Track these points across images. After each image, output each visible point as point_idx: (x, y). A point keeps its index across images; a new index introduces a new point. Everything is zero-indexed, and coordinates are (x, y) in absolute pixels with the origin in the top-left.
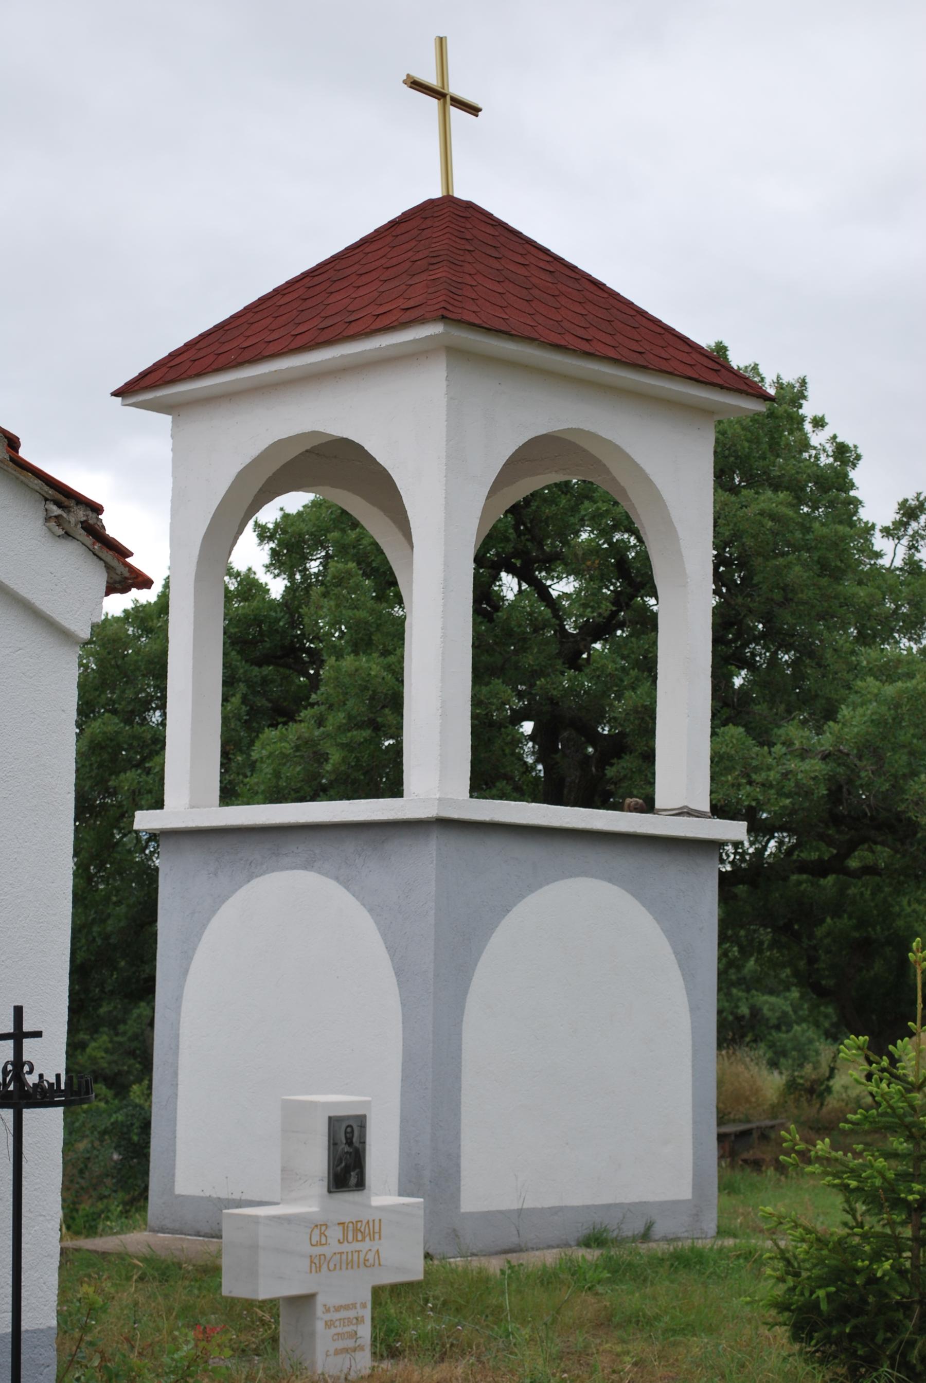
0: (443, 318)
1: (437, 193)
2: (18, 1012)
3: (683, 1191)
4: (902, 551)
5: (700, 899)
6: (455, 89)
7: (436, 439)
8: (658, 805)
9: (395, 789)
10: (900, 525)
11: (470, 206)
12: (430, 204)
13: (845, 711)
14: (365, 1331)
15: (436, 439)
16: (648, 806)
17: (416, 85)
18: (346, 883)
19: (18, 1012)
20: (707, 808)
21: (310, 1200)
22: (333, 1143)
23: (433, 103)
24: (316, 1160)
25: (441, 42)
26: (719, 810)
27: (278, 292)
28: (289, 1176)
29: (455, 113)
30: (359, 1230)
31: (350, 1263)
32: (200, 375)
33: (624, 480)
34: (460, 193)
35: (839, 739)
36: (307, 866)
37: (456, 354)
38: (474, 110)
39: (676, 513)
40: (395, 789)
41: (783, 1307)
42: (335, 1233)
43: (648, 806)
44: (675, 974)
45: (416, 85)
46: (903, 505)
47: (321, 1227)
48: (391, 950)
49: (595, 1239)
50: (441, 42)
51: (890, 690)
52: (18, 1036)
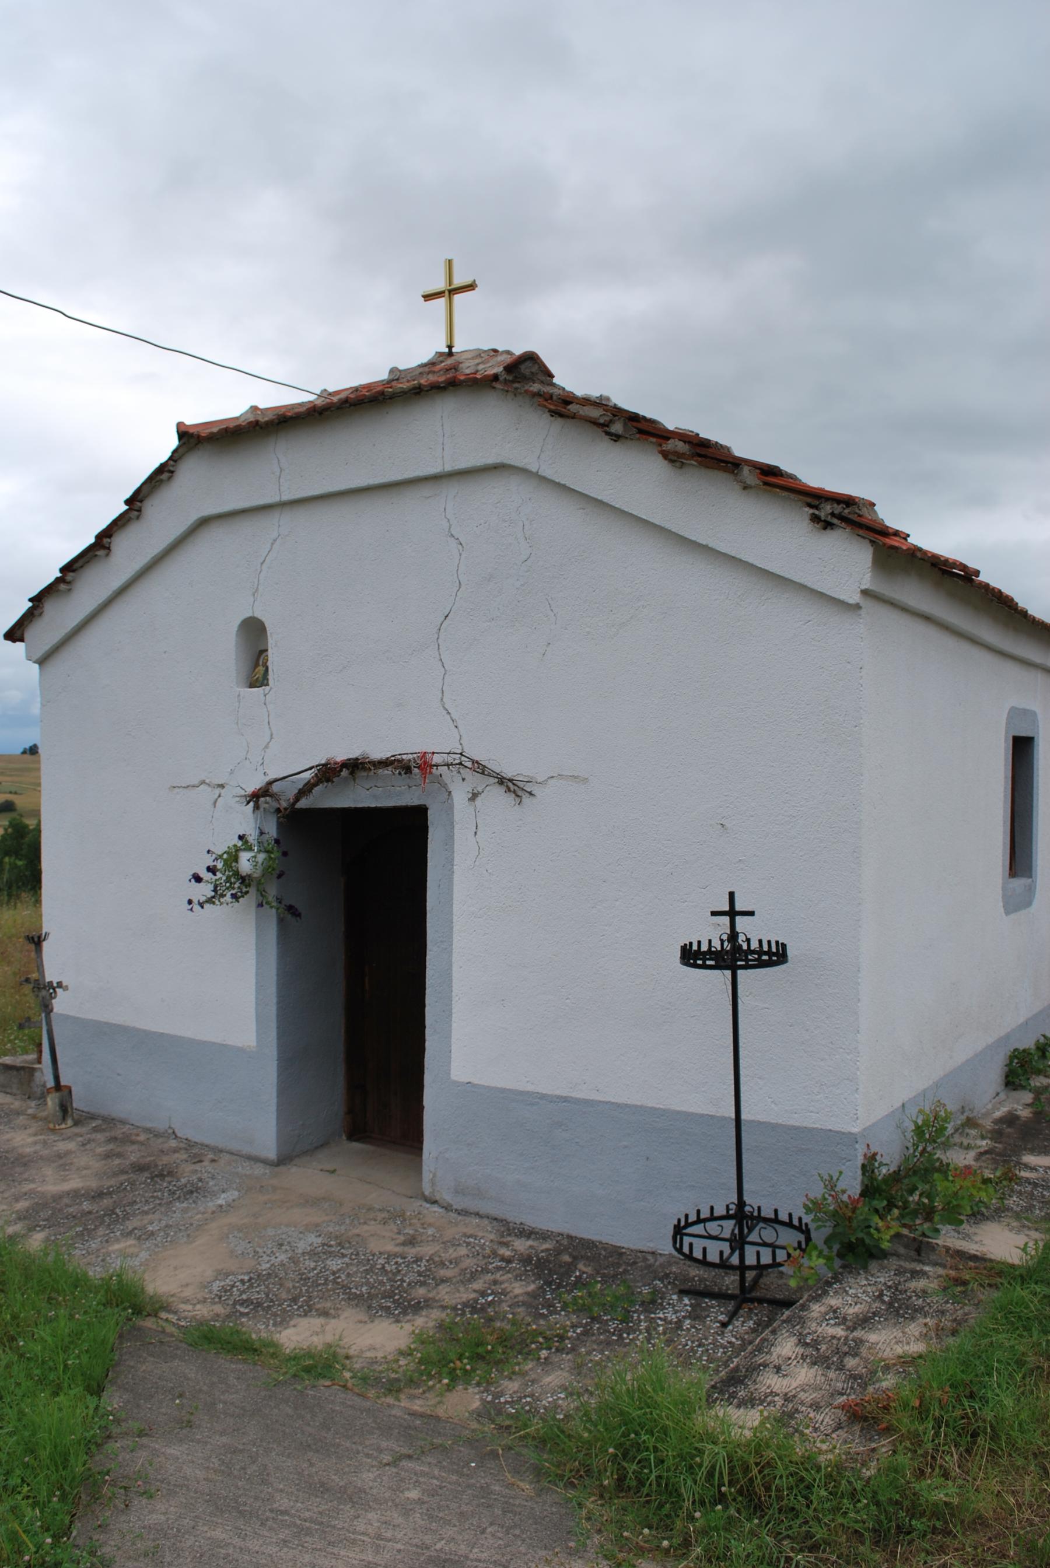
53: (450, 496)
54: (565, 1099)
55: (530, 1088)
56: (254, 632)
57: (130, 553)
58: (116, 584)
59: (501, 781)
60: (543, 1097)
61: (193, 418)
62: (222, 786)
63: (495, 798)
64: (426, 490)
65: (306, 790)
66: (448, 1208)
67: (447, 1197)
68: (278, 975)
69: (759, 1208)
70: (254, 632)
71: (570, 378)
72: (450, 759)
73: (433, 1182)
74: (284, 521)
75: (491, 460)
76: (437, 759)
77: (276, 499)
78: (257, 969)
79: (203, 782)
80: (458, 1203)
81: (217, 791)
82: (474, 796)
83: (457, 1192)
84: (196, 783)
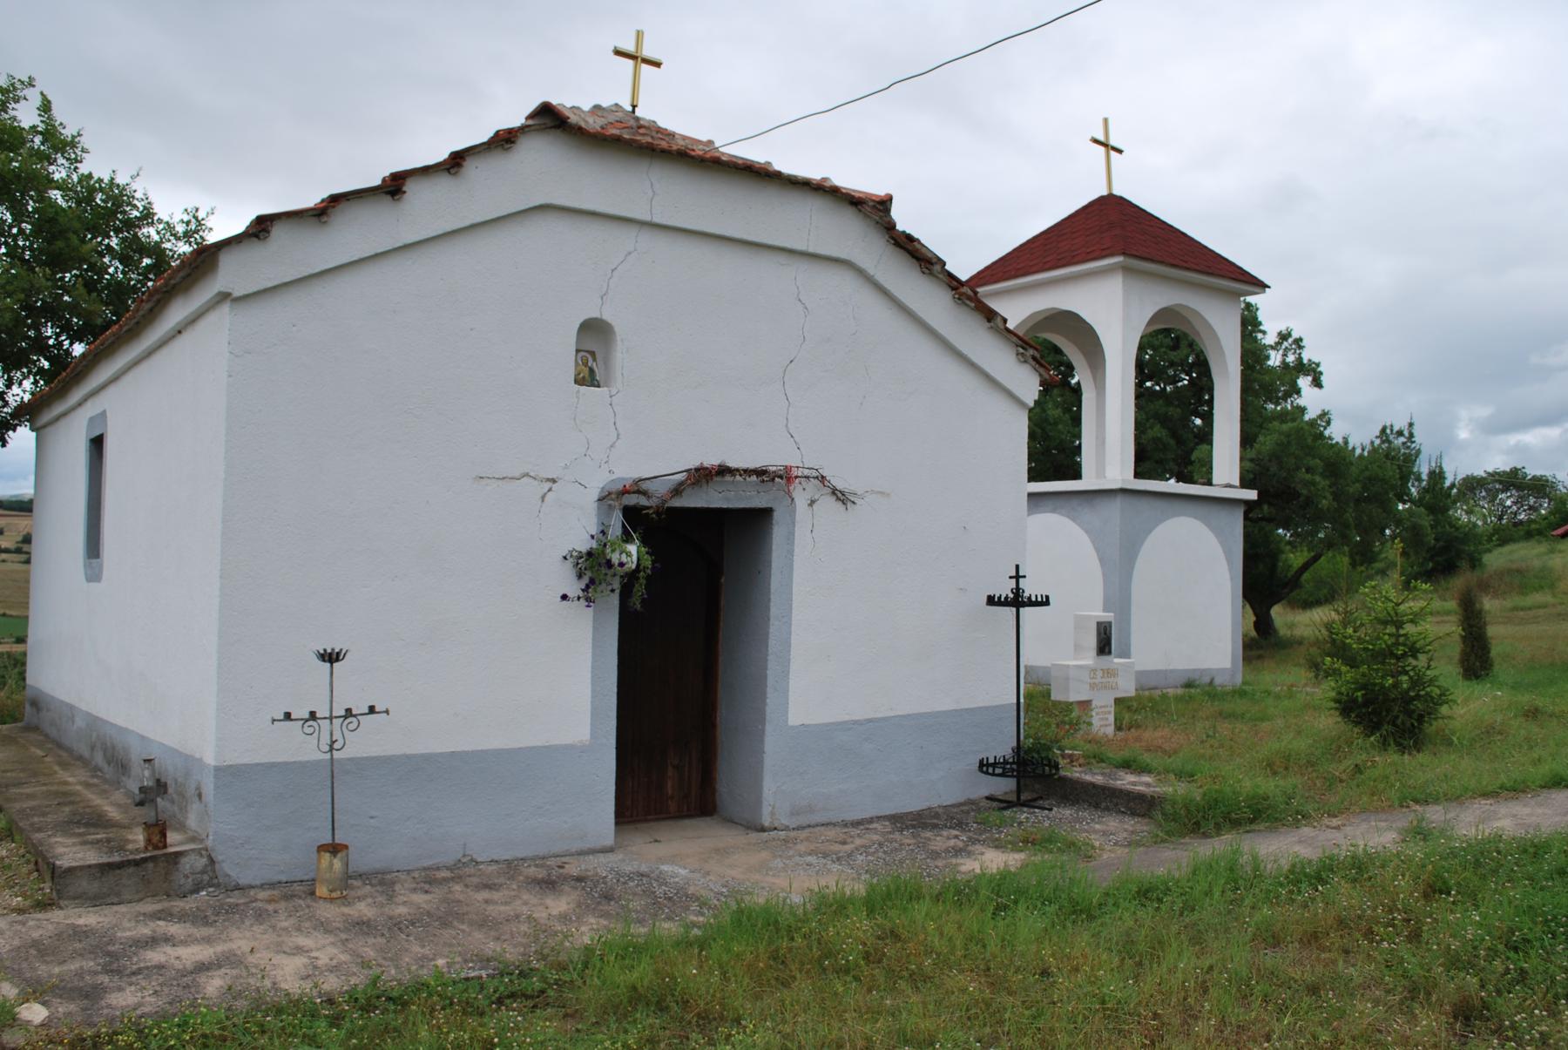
0: (1124, 254)
1: (1105, 193)
2: (1017, 567)
3: (1227, 664)
4: (1279, 358)
5: (1235, 524)
6: (1113, 142)
7: (1113, 310)
8: (1215, 481)
9: (1077, 475)
10: (1278, 344)
11: (1121, 198)
12: (1101, 200)
13: (1261, 438)
14: (1111, 718)
15: (1113, 310)
16: (1209, 483)
17: (1096, 141)
18: (1073, 520)
19: (1017, 567)
20: (1237, 483)
21: (1089, 658)
22: (1099, 634)
23: (1102, 149)
24: (1092, 641)
25: (1106, 121)
26: (1245, 484)
27: (1029, 242)
28: (1078, 648)
29: (1113, 153)
30: (1109, 673)
31: (1105, 687)
32: (996, 282)
33: (1198, 327)
34: (1116, 192)
35: (1259, 452)
36: (1053, 511)
37: (1126, 270)
38: (1120, 151)
39: (1224, 342)
40: (1077, 475)
41: (1337, 701)
42: (1100, 674)
43: (1209, 483)
44: (1224, 562)
45: (1096, 141)
46: (1280, 334)
47: (1094, 670)
48: (1097, 550)
49: (1189, 685)
50: (1106, 121)
51: (1285, 427)
52: (1017, 577)
53: (802, 270)
54: (870, 721)
55: (847, 718)
56: (595, 332)
57: (427, 210)
58: (881, 278)
59: (834, 491)
60: (855, 722)
61: (563, 99)
62: (554, 481)
63: (828, 504)
64: (782, 258)
65: (677, 491)
66: (786, 828)
67: (785, 821)
68: (765, 677)
69: (984, 766)
70: (595, 332)
71: (903, 218)
72: (806, 472)
73: (772, 814)
74: (646, 239)
75: (843, 256)
76: (795, 472)
77: (647, 218)
78: (594, 661)
79: (527, 475)
80: (793, 823)
81: (549, 485)
82: (812, 503)
83: (792, 814)
84: (517, 474)
